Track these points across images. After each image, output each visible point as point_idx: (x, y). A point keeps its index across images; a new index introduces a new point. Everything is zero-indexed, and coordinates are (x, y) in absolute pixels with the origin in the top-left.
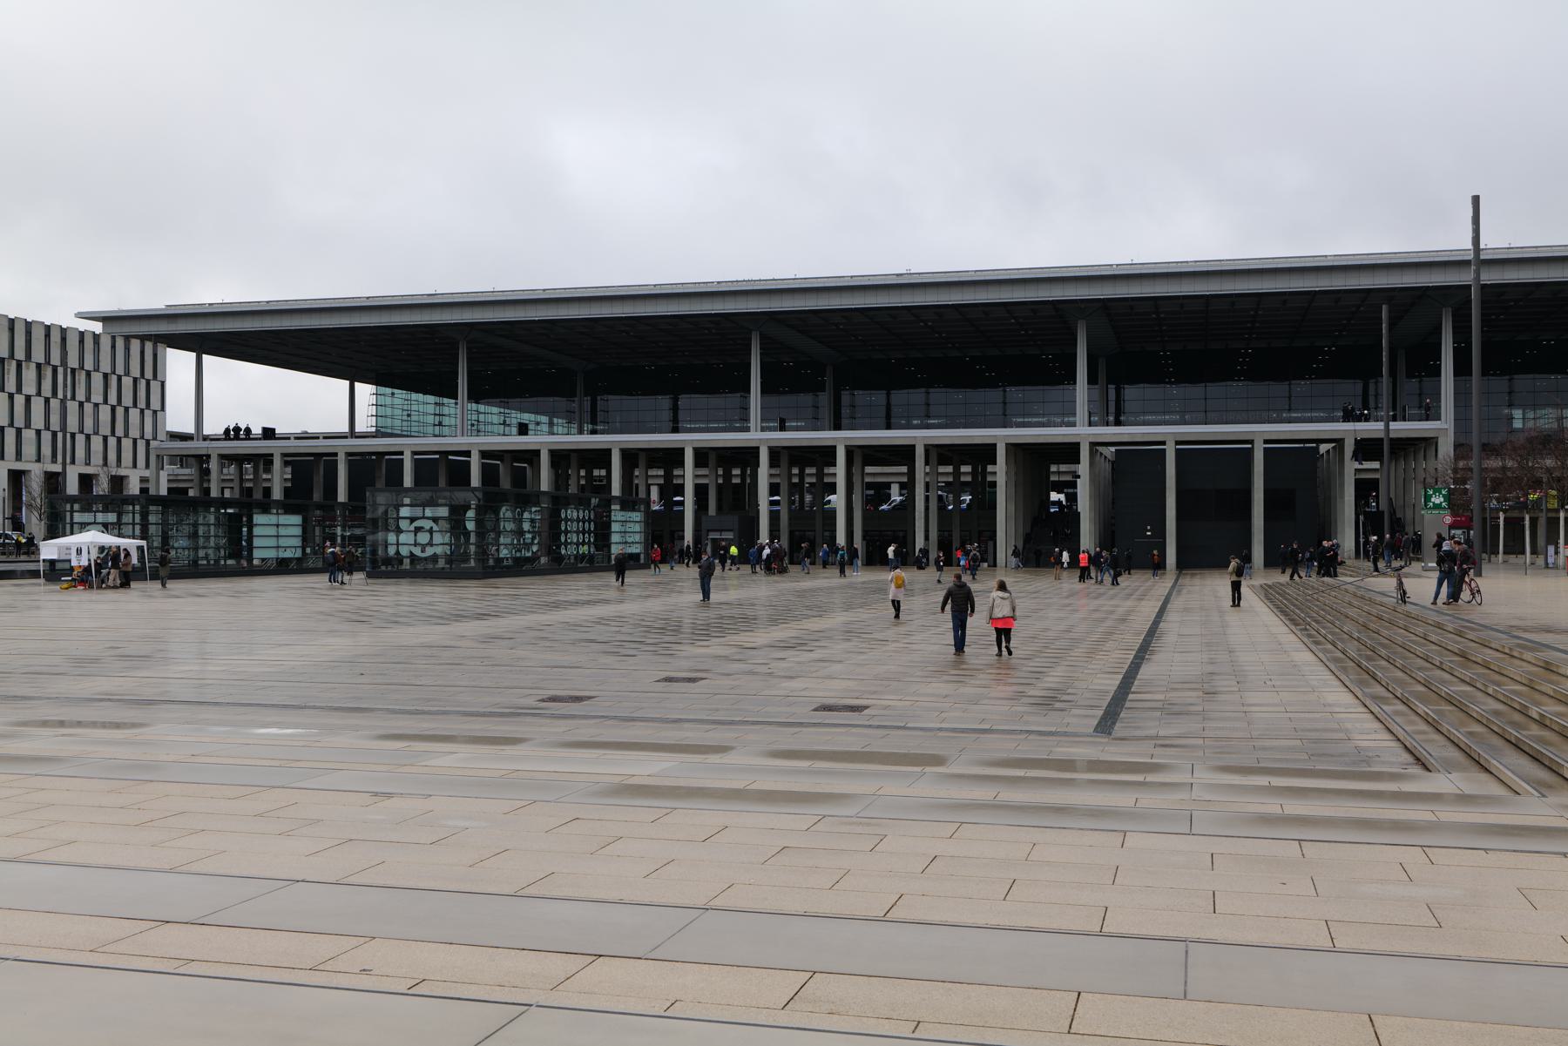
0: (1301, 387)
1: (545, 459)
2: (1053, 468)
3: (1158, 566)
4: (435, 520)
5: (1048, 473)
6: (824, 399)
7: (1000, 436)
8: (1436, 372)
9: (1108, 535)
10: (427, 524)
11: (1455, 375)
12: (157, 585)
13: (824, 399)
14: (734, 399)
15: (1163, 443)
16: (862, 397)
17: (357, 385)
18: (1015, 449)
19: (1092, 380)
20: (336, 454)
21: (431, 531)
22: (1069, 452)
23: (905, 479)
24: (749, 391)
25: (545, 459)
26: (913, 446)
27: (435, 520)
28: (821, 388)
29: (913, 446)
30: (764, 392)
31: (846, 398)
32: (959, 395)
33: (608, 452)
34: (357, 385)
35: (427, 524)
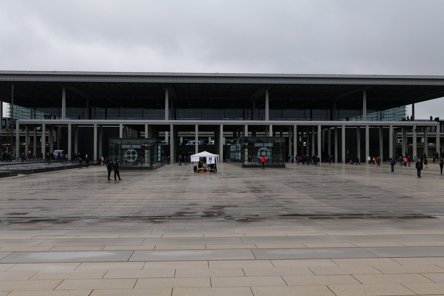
0: (227, 111)
1: (295, 128)
2: (179, 133)
3: (334, 162)
4: (268, 148)
5: (159, 134)
6: (86, 110)
7: (146, 122)
8: (264, 108)
9: (324, 154)
10: (265, 149)
11: (66, 107)
12: (388, 167)
13: (86, 110)
14: (56, 109)
15: (93, 125)
16: (98, 110)
17: (3, 102)
18: (150, 126)
19: (169, 108)
20: (67, 125)
21: (267, 152)
22: (166, 128)
23: (213, 136)
24: (61, 107)
25: (295, 128)
26: (170, 125)
27: (268, 148)
28: (84, 107)
29: (170, 125)
30: (67, 106)
31: (93, 110)
32: (128, 110)
33: (194, 126)
34: (3, 102)
35: (265, 149)
